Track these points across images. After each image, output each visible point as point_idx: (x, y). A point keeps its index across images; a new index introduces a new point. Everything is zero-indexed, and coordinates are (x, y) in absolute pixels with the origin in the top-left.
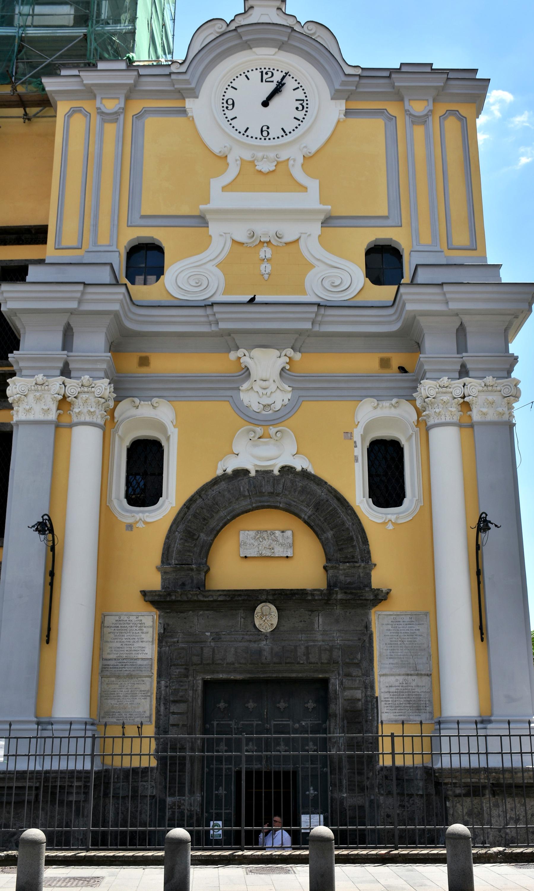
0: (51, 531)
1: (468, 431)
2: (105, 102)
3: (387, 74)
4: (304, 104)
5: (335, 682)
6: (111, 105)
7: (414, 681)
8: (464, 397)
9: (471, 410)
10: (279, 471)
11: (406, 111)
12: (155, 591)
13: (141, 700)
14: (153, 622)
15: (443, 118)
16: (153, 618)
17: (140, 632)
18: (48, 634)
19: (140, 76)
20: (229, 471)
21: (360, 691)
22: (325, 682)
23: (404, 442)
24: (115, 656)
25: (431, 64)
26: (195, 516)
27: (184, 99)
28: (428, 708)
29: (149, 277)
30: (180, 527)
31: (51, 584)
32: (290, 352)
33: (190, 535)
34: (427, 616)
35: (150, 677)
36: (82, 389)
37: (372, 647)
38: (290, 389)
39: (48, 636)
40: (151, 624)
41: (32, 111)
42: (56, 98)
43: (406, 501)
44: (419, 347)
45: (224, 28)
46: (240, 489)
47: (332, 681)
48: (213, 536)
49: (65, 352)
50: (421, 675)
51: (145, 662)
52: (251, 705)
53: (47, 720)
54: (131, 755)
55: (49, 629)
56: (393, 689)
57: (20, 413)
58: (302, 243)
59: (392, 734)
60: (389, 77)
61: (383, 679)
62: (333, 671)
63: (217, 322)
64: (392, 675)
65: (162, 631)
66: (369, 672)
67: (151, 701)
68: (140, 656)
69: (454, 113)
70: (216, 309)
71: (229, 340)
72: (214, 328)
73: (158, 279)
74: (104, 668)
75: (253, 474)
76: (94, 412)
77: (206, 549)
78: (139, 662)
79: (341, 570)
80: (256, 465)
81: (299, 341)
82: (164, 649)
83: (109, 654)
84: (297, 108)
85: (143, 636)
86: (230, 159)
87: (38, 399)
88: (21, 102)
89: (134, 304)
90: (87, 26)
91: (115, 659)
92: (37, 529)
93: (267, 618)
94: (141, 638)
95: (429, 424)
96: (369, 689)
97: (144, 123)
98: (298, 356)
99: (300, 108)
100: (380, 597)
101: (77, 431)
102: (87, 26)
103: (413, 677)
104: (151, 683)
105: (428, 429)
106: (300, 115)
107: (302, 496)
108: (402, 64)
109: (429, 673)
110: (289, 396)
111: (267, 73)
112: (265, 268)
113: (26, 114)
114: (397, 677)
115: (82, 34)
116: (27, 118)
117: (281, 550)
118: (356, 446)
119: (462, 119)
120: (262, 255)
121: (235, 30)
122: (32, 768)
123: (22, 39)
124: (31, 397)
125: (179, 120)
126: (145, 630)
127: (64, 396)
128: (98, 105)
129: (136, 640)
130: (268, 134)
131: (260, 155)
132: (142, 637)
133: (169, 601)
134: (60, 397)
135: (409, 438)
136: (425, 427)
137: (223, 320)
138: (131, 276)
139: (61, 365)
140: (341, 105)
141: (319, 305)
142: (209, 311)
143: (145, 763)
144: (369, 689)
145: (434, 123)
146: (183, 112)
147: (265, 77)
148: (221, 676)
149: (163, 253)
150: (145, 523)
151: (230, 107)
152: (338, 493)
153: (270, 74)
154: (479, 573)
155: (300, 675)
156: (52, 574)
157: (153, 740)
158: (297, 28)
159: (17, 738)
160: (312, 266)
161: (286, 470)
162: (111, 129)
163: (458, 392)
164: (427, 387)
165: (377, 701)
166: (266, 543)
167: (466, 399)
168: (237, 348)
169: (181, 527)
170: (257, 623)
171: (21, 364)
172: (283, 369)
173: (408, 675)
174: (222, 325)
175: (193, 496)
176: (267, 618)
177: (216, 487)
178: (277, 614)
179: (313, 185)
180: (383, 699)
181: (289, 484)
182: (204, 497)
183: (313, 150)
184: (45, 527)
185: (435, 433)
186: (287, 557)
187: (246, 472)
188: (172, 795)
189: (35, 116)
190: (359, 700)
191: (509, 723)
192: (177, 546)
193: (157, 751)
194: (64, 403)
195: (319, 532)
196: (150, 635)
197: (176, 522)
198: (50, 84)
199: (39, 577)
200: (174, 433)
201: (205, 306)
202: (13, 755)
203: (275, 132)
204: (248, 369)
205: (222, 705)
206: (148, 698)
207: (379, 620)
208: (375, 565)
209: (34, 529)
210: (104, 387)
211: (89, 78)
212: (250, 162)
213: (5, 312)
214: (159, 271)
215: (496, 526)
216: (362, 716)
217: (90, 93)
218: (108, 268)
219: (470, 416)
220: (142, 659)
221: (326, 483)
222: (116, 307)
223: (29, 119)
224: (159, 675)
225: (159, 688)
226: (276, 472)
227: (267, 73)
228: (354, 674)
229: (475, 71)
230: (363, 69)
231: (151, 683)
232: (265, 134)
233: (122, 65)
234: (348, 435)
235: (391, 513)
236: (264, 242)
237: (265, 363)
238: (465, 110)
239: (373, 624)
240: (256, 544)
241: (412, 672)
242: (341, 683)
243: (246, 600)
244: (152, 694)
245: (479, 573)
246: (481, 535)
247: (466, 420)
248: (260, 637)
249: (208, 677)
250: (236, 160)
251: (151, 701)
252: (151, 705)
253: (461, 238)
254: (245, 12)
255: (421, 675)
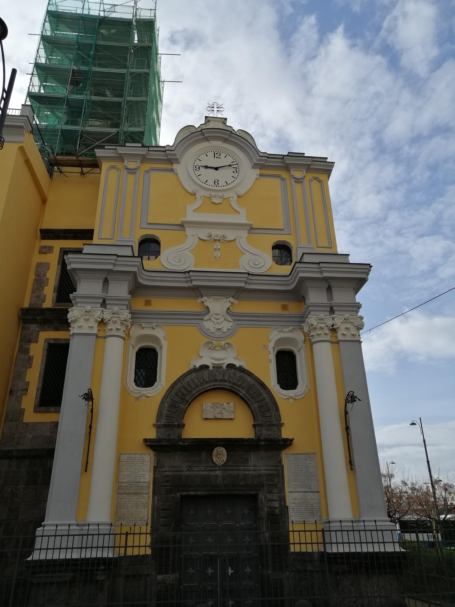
0: (92, 399)
1: (335, 345)
2: (129, 163)
3: (282, 157)
4: (237, 170)
5: (261, 496)
6: (132, 165)
7: (310, 496)
8: (333, 326)
9: (337, 333)
10: (226, 367)
11: (292, 176)
12: (153, 439)
13: (142, 510)
14: (150, 458)
15: (310, 181)
16: (151, 456)
17: (142, 465)
18: (86, 466)
19: (149, 150)
20: (197, 366)
21: (277, 502)
22: (255, 497)
23: (296, 352)
24: (126, 481)
25: (304, 154)
26: (176, 394)
27: (172, 164)
28: (318, 513)
29: (151, 257)
30: (167, 400)
31: (90, 433)
32: (232, 300)
33: (173, 405)
34: (317, 454)
35: (148, 494)
36: (113, 315)
37: (284, 474)
38: (232, 320)
39: (86, 467)
40: (149, 460)
41: (85, 170)
42: (102, 160)
43: (299, 386)
44: (304, 299)
45: (195, 130)
46: (203, 377)
47: (260, 496)
48: (187, 405)
49: (104, 294)
50: (313, 492)
51: (145, 484)
52: (210, 512)
53: (83, 523)
54: (139, 547)
55: (87, 462)
56: (297, 501)
57: (75, 329)
58: (237, 240)
59: (127, 532)
60: (283, 158)
61: (291, 494)
62: (260, 490)
63: (191, 281)
64: (296, 492)
65: (156, 465)
66: (282, 490)
67: (148, 510)
68: (142, 480)
69: (316, 179)
70: (191, 274)
71: (196, 291)
72: (189, 284)
73: (156, 258)
74: (119, 488)
75: (211, 368)
76: (120, 329)
77: (183, 413)
78: (141, 484)
79: (264, 426)
80: (213, 363)
81: (239, 293)
82: (157, 475)
83: (123, 479)
84: (234, 172)
85: (144, 467)
86: (197, 196)
87: (87, 320)
88: (80, 165)
89: (144, 269)
90: (119, 128)
91: (126, 482)
92: (84, 397)
93: (220, 456)
94: (143, 469)
95: (313, 341)
96: (283, 501)
97: (150, 175)
98: (236, 302)
99: (235, 172)
100: (287, 443)
101: (110, 340)
102: (119, 128)
103: (309, 494)
104: (149, 497)
105: (312, 344)
106: (235, 175)
107: (236, 383)
108: (289, 153)
109: (318, 490)
110: (232, 324)
111: (217, 154)
112: (218, 254)
113: (82, 171)
114: (299, 494)
115: (116, 132)
116: (82, 173)
117: (228, 414)
118: (270, 354)
119: (320, 181)
120: (215, 247)
121: (201, 131)
122: (83, 556)
123: (82, 131)
124: (82, 320)
125: (170, 174)
126: (145, 463)
127: (102, 319)
128: (125, 164)
129: (140, 470)
130: (218, 184)
131: (214, 194)
132: (144, 468)
133: (161, 445)
134: (100, 320)
135: (299, 351)
136: (310, 343)
137: (195, 280)
138: (140, 256)
139: (101, 301)
140: (258, 171)
141: (249, 274)
142: (187, 275)
143: (142, 552)
144: (283, 501)
145: (306, 182)
146: (172, 170)
147: (216, 155)
148: (192, 493)
149: (160, 244)
150: (146, 396)
151: (198, 169)
152: (261, 381)
153: (219, 154)
154: (347, 428)
155: (241, 492)
156: (90, 427)
157: (149, 536)
158: (233, 132)
159: (382, 531)
160: (244, 254)
161: (231, 366)
162: (131, 177)
163: (330, 323)
164: (312, 320)
165: (288, 509)
166: (218, 410)
167: (334, 327)
168: (202, 297)
169: (168, 400)
170: (214, 460)
171: (77, 300)
172: (228, 309)
173: (305, 492)
174: (195, 283)
175: (176, 381)
176: (220, 456)
177: (189, 376)
178: (226, 454)
179: (243, 212)
180: (291, 508)
181: (232, 375)
182: (182, 382)
183: (242, 193)
184: (89, 397)
185: (315, 346)
186: (231, 419)
187: (206, 367)
188: (160, 574)
189: (87, 173)
190: (277, 508)
191: (375, 521)
192: (165, 412)
193: (151, 543)
194: (102, 323)
195: (250, 404)
196: (149, 466)
197: (165, 397)
198: (99, 153)
199: (83, 430)
200: (164, 343)
201: (185, 272)
202: (70, 548)
203: (222, 183)
204: (208, 308)
205: (192, 512)
206: (147, 508)
207: (287, 458)
208: (284, 424)
209: (82, 397)
210: (126, 315)
211: (121, 150)
212: (208, 197)
213: (69, 270)
214: (157, 254)
215: (359, 400)
216: (278, 518)
217: (121, 158)
218: (131, 248)
219: (336, 337)
220: (143, 482)
221: (253, 374)
222: (135, 269)
223: (84, 174)
224: (154, 493)
225: (153, 501)
226: (224, 367)
227: (217, 154)
228: (274, 492)
229: (327, 158)
230: (268, 154)
231: (149, 497)
232: (216, 184)
233: (140, 145)
234: (265, 347)
235: (291, 393)
236: (216, 240)
237: (218, 306)
238: (322, 177)
239: (283, 460)
240: (212, 411)
241: (308, 490)
242: (266, 497)
243: (206, 446)
244: (149, 505)
245: (347, 428)
246: (349, 405)
247: (334, 340)
248: (216, 468)
249: (184, 493)
250: (201, 196)
251: (148, 510)
252: (148, 513)
253: (323, 242)
254: (205, 123)
255: (313, 492)
